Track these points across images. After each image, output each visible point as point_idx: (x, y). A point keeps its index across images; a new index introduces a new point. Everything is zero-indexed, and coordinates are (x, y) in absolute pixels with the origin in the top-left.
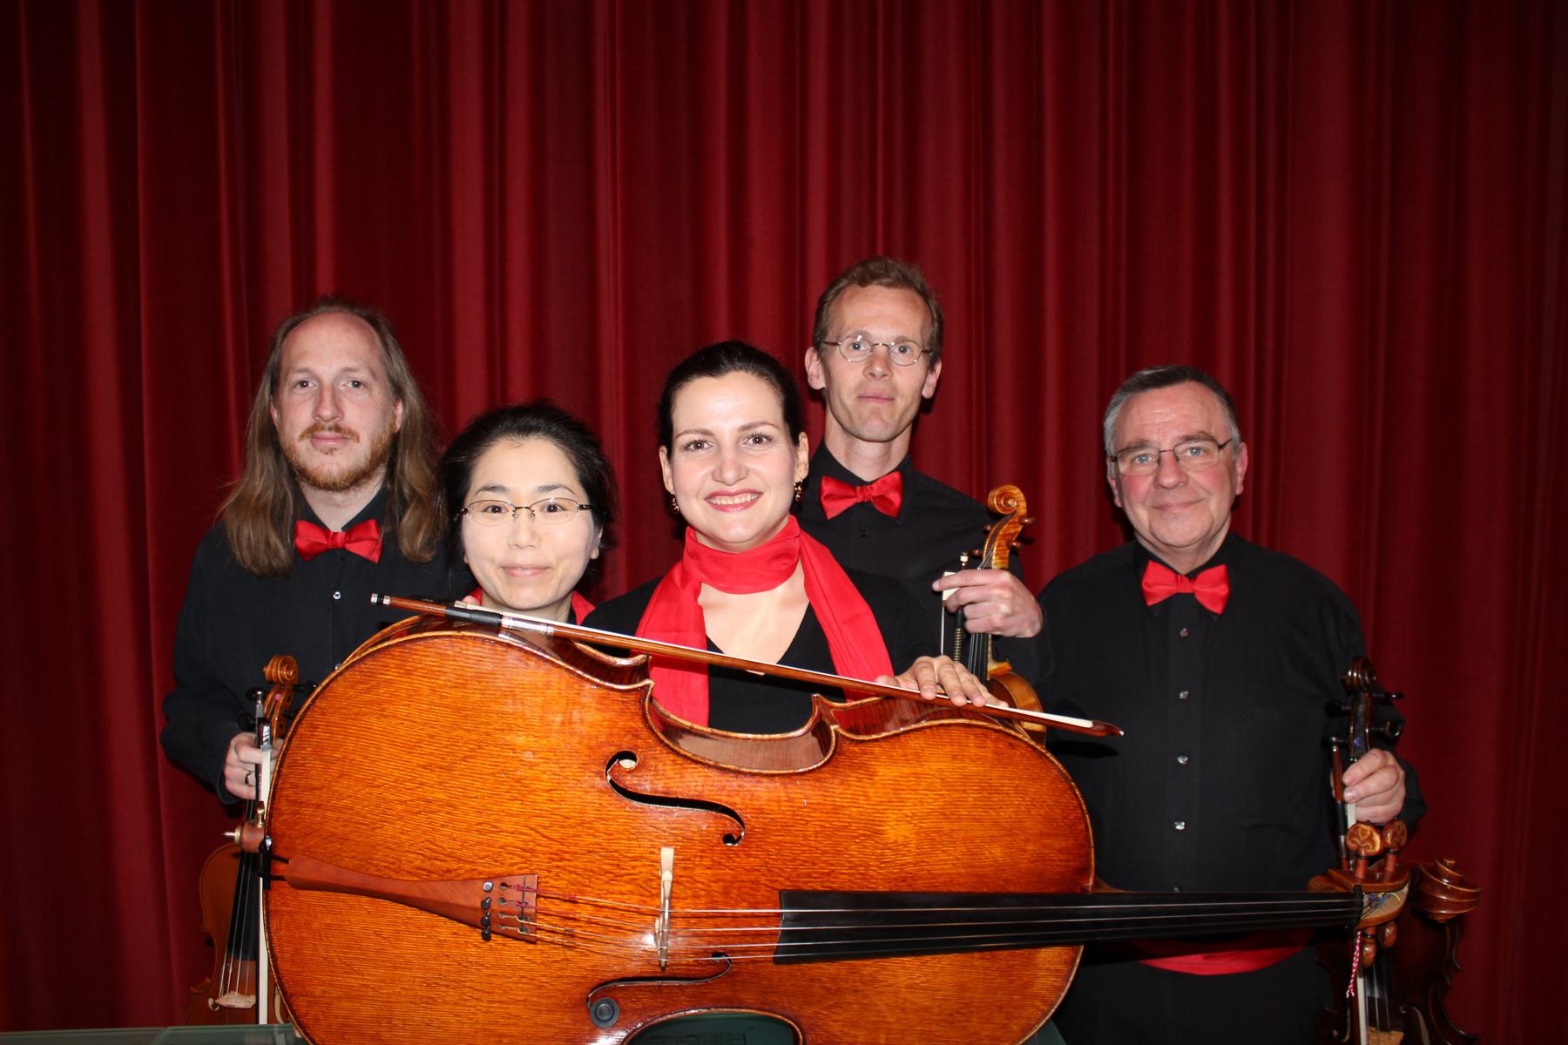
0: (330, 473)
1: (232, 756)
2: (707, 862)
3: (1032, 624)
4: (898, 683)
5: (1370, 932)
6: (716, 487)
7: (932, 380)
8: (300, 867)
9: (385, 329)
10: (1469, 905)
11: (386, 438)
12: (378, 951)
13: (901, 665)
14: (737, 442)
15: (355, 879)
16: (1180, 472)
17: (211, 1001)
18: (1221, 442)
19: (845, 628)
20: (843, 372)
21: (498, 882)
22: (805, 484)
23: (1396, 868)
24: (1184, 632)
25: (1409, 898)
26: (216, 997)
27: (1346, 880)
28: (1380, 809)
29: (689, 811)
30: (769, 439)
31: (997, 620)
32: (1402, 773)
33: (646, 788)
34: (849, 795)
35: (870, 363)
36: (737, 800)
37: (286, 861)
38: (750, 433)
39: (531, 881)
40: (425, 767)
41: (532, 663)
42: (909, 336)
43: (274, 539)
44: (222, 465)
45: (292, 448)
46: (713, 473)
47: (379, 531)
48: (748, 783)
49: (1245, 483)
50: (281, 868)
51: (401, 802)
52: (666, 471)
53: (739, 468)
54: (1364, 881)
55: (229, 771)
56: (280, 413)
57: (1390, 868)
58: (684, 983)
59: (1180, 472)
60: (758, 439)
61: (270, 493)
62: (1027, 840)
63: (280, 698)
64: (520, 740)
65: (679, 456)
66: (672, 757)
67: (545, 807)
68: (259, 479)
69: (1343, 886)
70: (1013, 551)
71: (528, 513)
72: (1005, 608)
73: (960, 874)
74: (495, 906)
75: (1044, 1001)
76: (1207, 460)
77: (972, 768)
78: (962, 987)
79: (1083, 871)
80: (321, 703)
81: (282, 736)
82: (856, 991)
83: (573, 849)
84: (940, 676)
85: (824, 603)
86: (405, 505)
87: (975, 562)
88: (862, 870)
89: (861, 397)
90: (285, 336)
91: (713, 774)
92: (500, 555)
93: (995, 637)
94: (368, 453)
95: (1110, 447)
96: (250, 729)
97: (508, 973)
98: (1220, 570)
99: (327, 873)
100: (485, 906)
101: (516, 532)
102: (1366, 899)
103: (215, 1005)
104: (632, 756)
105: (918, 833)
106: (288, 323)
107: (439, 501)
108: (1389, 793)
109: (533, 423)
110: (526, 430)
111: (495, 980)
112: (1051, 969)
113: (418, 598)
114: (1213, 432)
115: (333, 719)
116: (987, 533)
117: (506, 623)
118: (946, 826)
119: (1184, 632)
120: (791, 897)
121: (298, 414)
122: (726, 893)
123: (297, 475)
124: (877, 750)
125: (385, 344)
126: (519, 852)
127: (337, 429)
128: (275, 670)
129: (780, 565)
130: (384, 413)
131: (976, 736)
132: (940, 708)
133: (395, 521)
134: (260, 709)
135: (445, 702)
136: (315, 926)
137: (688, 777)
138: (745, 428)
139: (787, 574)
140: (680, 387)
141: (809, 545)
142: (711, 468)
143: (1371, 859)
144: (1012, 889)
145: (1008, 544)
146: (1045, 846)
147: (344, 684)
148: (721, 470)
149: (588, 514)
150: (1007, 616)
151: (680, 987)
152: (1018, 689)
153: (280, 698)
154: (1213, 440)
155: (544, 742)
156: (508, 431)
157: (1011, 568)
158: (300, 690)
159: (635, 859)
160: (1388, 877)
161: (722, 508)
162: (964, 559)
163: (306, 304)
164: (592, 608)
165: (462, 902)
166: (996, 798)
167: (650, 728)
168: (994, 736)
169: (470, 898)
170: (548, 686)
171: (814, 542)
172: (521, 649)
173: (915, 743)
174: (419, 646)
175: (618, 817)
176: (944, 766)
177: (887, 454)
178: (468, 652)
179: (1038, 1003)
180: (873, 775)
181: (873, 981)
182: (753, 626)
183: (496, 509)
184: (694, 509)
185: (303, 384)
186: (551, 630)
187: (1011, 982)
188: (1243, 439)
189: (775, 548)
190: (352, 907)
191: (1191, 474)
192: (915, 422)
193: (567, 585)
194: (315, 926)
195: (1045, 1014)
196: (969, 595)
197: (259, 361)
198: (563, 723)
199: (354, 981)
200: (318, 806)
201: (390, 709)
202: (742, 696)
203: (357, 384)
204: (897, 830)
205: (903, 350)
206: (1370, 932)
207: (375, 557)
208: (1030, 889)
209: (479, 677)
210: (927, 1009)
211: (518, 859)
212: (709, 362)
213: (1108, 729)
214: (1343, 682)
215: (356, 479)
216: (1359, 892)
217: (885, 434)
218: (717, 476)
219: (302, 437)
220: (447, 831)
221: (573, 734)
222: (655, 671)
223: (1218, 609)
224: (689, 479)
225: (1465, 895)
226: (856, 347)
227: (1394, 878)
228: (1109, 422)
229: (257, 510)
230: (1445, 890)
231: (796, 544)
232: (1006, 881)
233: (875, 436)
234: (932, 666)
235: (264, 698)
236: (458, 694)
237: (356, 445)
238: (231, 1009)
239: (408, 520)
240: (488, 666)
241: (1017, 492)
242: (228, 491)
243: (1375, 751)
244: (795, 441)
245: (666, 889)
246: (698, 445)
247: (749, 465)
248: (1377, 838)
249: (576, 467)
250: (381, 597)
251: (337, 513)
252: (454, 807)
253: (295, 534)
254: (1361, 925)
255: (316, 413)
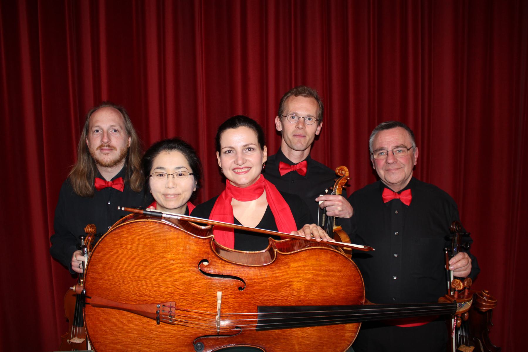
0: (107, 161)
1: (74, 258)
2: (233, 296)
3: (349, 214)
4: (298, 234)
5: (459, 316)
6: (235, 166)
7: (319, 128)
8: (95, 299)
9: (124, 112)
10: (493, 306)
11: (125, 149)
12: (122, 328)
13: (300, 226)
14: (243, 150)
15: (113, 304)
16: (394, 158)
17: (68, 341)
18: (409, 148)
19: (279, 212)
20: (289, 126)
21: (162, 305)
22: (266, 163)
23: (468, 294)
24: (396, 212)
25: (473, 304)
26: (70, 339)
27: (451, 298)
28: (462, 273)
29: (227, 279)
30: (253, 149)
31: (337, 212)
32: (470, 260)
33: (212, 272)
34: (280, 273)
35: (298, 123)
36: (243, 275)
37: (90, 298)
38: (247, 147)
39: (173, 304)
40: (136, 265)
41: (172, 230)
42: (312, 114)
43: (88, 184)
44: (71, 160)
45: (94, 153)
46: (234, 162)
47: (123, 181)
48: (247, 269)
49: (417, 161)
50: (89, 300)
51: (129, 278)
52: (219, 160)
53: (243, 159)
54: (457, 299)
55: (73, 263)
56: (89, 141)
57: (466, 294)
58: (226, 337)
59: (394, 158)
60: (250, 149)
61: (86, 169)
62: (342, 287)
63: (90, 238)
64: (169, 256)
65: (223, 155)
66: (221, 261)
67: (178, 278)
68: (82, 164)
69: (450, 301)
70: (343, 189)
71: (172, 176)
72: (339, 208)
73: (319, 299)
74: (161, 313)
75: (348, 341)
76: (404, 154)
77: (323, 263)
78: (320, 337)
79: (361, 297)
80: (101, 244)
81: (90, 251)
82: (284, 339)
83: (187, 292)
84: (313, 231)
85: (273, 205)
86: (132, 172)
87: (329, 193)
88: (286, 298)
89: (294, 135)
90: (90, 115)
91: (235, 266)
92: (163, 190)
93: (336, 218)
94: (120, 154)
95: (372, 150)
96: (80, 249)
97: (167, 334)
98: (409, 191)
99: (104, 302)
100: (158, 313)
101: (168, 183)
102: (458, 304)
103: (70, 342)
104: (207, 261)
105: (305, 286)
106: (91, 111)
107: (141, 172)
108: (465, 267)
109: (174, 146)
110: (171, 148)
111: (162, 337)
112: (351, 331)
113: (134, 208)
114: (406, 144)
115: (105, 250)
116: (335, 182)
117: (164, 215)
118: (314, 283)
119: (396, 212)
120: (261, 308)
121: (95, 141)
122: (240, 306)
123: (95, 162)
124: (290, 257)
125: (125, 117)
126: (169, 294)
127: (109, 146)
128: (88, 229)
129: (258, 191)
130: (125, 141)
131: (324, 252)
132: (313, 242)
133: (129, 178)
134: (83, 243)
135: (143, 243)
136: (101, 319)
137: (226, 268)
138: (245, 146)
139: (260, 194)
140: (223, 132)
141: (268, 184)
142: (233, 160)
143: (459, 291)
144: (337, 304)
145: (342, 186)
146: (348, 289)
147: (109, 238)
148: (237, 160)
149: (192, 176)
150: (340, 211)
151: (225, 338)
152: (343, 236)
153: (90, 238)
154: (406, 147)
155: (177, 256)
156: (164, 148)
157: (342, 195)
158: (97, 236)
159: (208, 296)
160: (465, 297)
161: (238, 173)
162: (327, 191)
163: (98, 104)
164: (195, 207)
165: (150, 311)
166: (331, 273)
167: (213, 251)
168: (330, 252)
169: (152, 310)
170: (178, 237)
171: (270, 183)
172: (169, 225)
173: (304, 255)
174: (134, 225)
175: (203, 281)
176: (313, 263)
177: (302, 155)
178: (150, 226)
179: (346, 342)
180: (289, 266)
181: (290, 335)
182: (249, 213)
183: (161, 175)
184: (229, 174)
185: (97, 131)
186: (179, 218)
187: (337, 335)
188: (417, 146)
189: (256, 186)
190: (113, 313)
191: (398, 159)
192: (312, 145)
193: (185, 201)
194: (101, 319)
195: (349, 345)
196: (327, 203)
197: (82, 124)
198: (183, 250)
199: (114, 338)
200: (101, 279)
201: (125, 246)
202: (246, 239)
203: (115, 131)
204: (297, 285)
205: (309, 119)
206: (459, 316)
207: (122, 190)
208: (343, 304)
209: (154, 235)
210: (309, 344)
211: (169, 296)
212: (232, 123)
213: (369, 248)
214: (450, 229)
215: (116, 163)
216: (455, 303)
217: (302, 149)
218: (236, 162)
219: (97, 149)
220: (145, 287)
221: (187, 254)
222: (215, 231)
223: (408, 204)
224: (226, 163)
225: (492, 303)
226: (293, 118)
227: (467, 297)
228: (371, 140)
229: (82, 174)
230: (485, 301)
231: (263, 184)
232: (335, 301)
233: (299, 149)
234: (310, 228)
235: (84, 239)
236: (148, 240)
237: (116, 152)
238: (75, 343)
239: (133, 177)
240: (157, 231)
241: (345, 168)
242: (71, 168)
243: (460, 253)
244: (262, 149)
245: (219, 306)
246: (229, 152)
247: (247, 158)
248: (462, 284)
249: (188, 160)
250: (121, 208)
251: (109, 174)
252: (147, 279)
253: (95, 182)
254: (456, 314)
255: (102, 141)
